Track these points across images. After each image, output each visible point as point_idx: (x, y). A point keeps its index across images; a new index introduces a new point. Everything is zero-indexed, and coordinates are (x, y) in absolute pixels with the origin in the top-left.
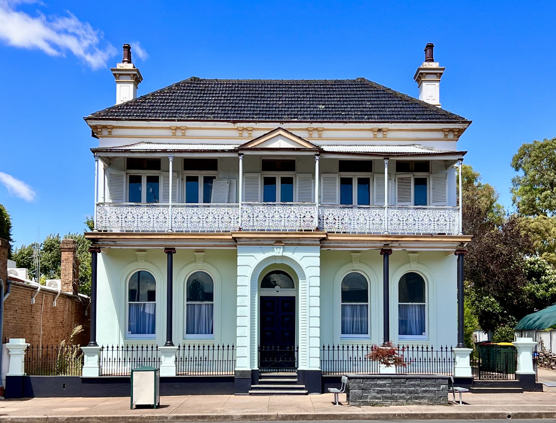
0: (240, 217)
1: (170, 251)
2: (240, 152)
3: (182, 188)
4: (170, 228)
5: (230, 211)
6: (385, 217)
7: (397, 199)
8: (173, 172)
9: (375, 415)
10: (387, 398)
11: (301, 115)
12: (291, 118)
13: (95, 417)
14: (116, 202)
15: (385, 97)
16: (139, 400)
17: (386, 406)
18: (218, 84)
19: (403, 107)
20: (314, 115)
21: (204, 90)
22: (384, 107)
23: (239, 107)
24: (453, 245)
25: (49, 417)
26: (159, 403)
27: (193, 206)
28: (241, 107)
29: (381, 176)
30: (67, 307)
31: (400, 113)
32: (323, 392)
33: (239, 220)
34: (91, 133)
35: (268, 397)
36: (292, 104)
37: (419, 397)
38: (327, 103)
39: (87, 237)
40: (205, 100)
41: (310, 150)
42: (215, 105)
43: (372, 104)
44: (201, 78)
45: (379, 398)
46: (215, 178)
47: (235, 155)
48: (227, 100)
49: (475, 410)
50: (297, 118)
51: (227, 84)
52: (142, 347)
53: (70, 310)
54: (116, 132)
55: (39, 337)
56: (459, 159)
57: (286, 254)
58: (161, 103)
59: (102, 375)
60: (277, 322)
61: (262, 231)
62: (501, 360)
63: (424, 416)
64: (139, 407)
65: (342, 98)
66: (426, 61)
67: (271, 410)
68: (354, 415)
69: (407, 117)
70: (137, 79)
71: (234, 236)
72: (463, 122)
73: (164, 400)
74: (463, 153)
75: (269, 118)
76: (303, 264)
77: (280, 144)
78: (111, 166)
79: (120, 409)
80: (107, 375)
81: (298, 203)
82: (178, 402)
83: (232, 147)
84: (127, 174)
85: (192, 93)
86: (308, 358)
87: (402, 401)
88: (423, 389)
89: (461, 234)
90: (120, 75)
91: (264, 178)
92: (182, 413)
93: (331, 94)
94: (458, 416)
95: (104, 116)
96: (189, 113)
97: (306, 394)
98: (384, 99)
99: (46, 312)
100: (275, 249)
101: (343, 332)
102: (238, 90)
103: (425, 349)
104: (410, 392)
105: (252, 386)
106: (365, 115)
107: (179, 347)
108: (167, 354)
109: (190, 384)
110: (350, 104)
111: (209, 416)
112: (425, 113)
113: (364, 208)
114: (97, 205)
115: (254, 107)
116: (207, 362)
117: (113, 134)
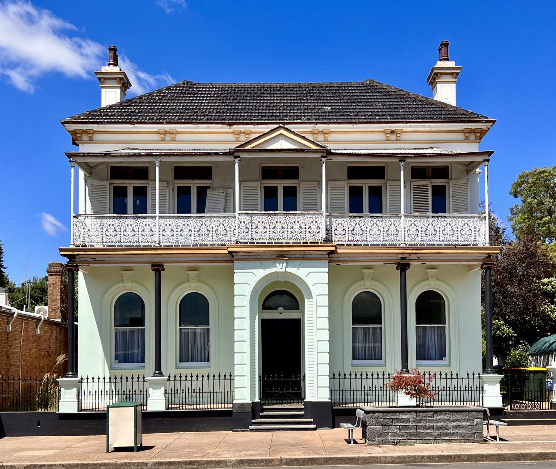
0: (237, 228)
1: (158, 268)
3: (173, 199)
4: (157, 242)
5: (226, 222)
6: (400, 228)
8: (160, 181)
9: (399, 457)
10: (411, 435)
11: (304, 116)
12: (294, 119)
13: (60, 465)
14: (98, 213)
15: (397, 98)
16: (116, 443)
17: (410, 445)
18: (213, 88)
19: (417, 108)
20: (319, 116)
21: (198, 94)
22: (397, 108)
23: (235, 109)
24: (479, 258)
25: (5, 464)
26: (141, 444)
27: (183, 217)
28: (238, 109)
29: (394, 183)
30: (55, 335)
31: (415, 113)
32: (334, 427)
33: (236, 233)
34: (71, 140)
35: (270, 433)
36: (294, 106)
38: (333, 104)
39: (62, 253)
40: (198, 103)
41: (315, 151)
42: (209, 107)
43: (383, 105)
44: (194, 82)
45: (402, 436)
46: (209, 187)
47: (230, 159)
48: (223, 103)
49: (519, 449)
50: (300, 119)
51: (222, 88)
52: (127, 378)
53: (58, 338)
54: (97, 137)
55: (18, 367)
56: (485, 160)
57: (289, 270)
58: (149, 106)
59: (81, 410)
60: (281, 347)
61: (261, 244)
62: (531, 386)
63: (459, 458)
64: (117, 449)
65: (350, 99)
66: (441, 60)
67: (273, 452)
68: (373, 457)
69: (423, 116)
70: (125, 84)
71: (230, 249)
72: (487, 122)
73: (148, 439)
74: (490, 153)
75: (268, 120)
76: (309, 281)
77: (281, 145)
78: (93, 175)
79: (95, 453)
80: (90, 410)
81: (303, 212)
82: (165, 441)
84: (111, 184)
85: (183, 97)
86: (317, 387)
87: (429, 438)
89: (488, 245)
90: (105, 79)
91: (265, 187)
92: (166, 458)
93: (337, 96)
94: (500, 457)
95: (83, 119)
96: (179, 116)
97: (315, 429)
98: (396, 100)
99: (27, 340)
100: (277, 264)
101: (354, 358)
102: (234, 93)
103: (449, 376)
104: (439, 428)
105: (253, 421)
106: (376, 115)
107: (169, 377)
108: (156, 385)
109: (182, 420)
110: (358, 105)
111: (197, 462)
112: (443, 112)
113: (378, 217)
114: (74, 217)
115: (252, 109)
116: (201, 394)
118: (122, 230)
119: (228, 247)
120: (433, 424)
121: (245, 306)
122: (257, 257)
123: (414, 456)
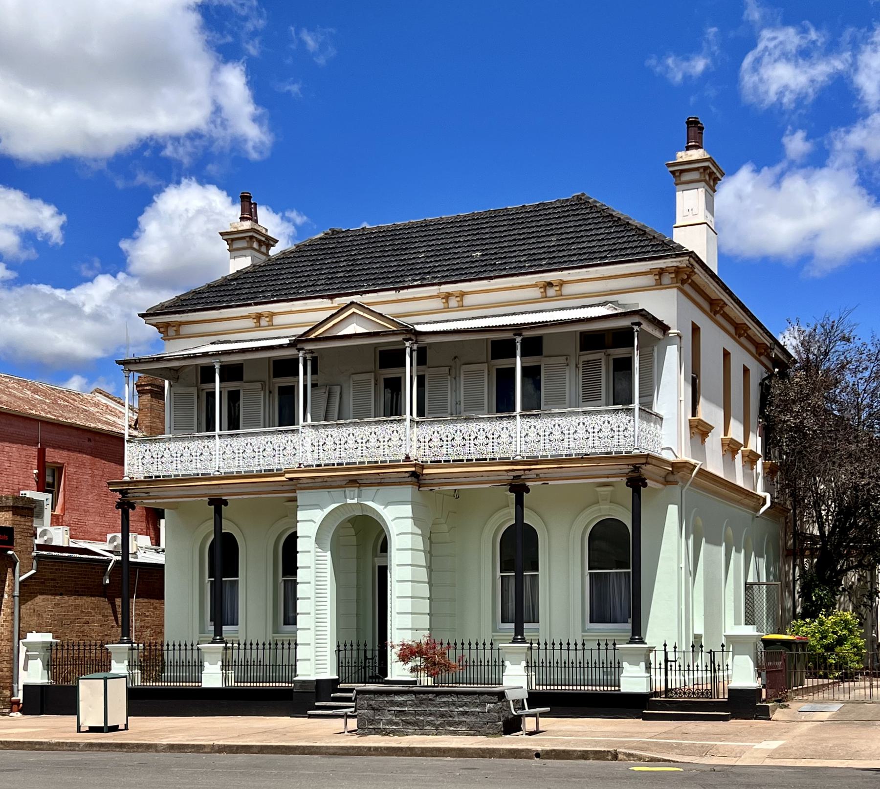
2: (299, 346)
7: (581, 398)
16: (86, 723)
27: (286, 431)
37: (456, 722)
41: (393, 333)
45: (397, 724)
54: (185, 330)
64: (92, 729)
83: (286, 341)
88: (461, 709)
90: (682, 171)
104: (442, 715)
105: (317, 704)
117: (181, 333)
118: (596, 430)
119: (286, 472)
120: (435, 709)
121: (398, 550)
122: (324, 484)
123: (359, 747)
